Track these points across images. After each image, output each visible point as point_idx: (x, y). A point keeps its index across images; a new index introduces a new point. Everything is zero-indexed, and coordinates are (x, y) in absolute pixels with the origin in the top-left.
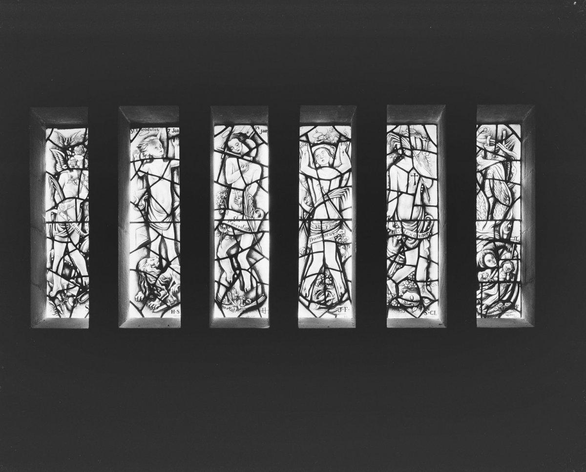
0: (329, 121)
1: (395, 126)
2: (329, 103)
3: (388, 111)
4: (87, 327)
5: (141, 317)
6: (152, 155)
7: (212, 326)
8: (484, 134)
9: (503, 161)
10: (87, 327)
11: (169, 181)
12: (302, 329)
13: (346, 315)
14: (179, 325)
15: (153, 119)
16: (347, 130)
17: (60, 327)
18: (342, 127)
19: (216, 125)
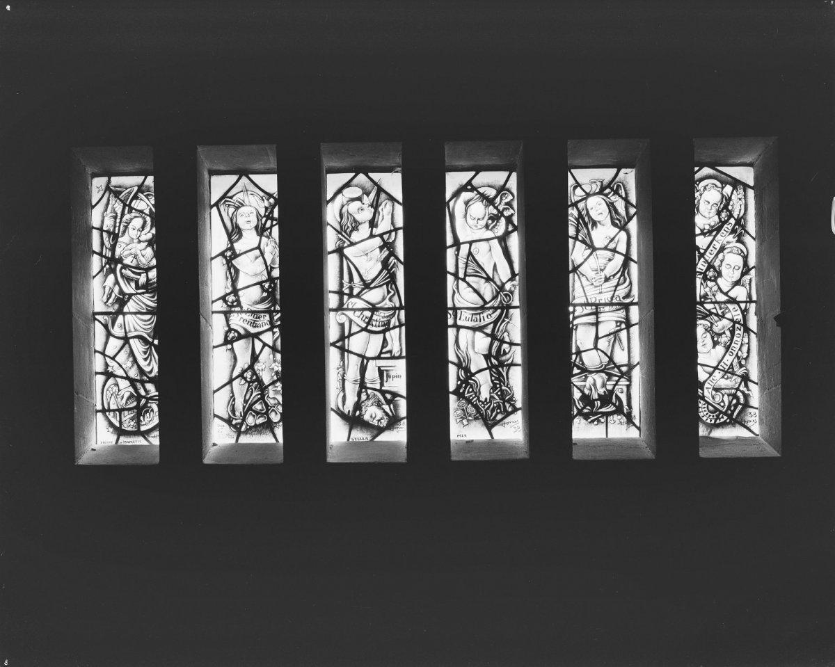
0: (228, 168)
1: (354, 174)
2: (487, 142)
3: (446, 155)
4: (404, 461)
5: (489, 438)
6: (239, 207)
7: (577, 455)
8: (585, 179)
9: (725, 203)
10: (157, 460)
11: (619, 232)
12: (576, 460)
13: (512, 431)
14: (402, 457)
15: (130, 168)
16: (150, 181)
17: (392, 461)
18: (726, 168)
19: (213, 173)
